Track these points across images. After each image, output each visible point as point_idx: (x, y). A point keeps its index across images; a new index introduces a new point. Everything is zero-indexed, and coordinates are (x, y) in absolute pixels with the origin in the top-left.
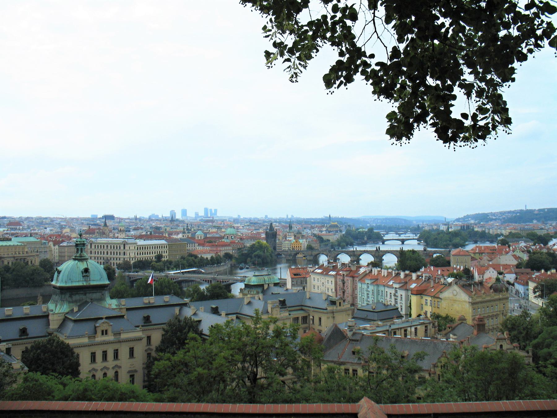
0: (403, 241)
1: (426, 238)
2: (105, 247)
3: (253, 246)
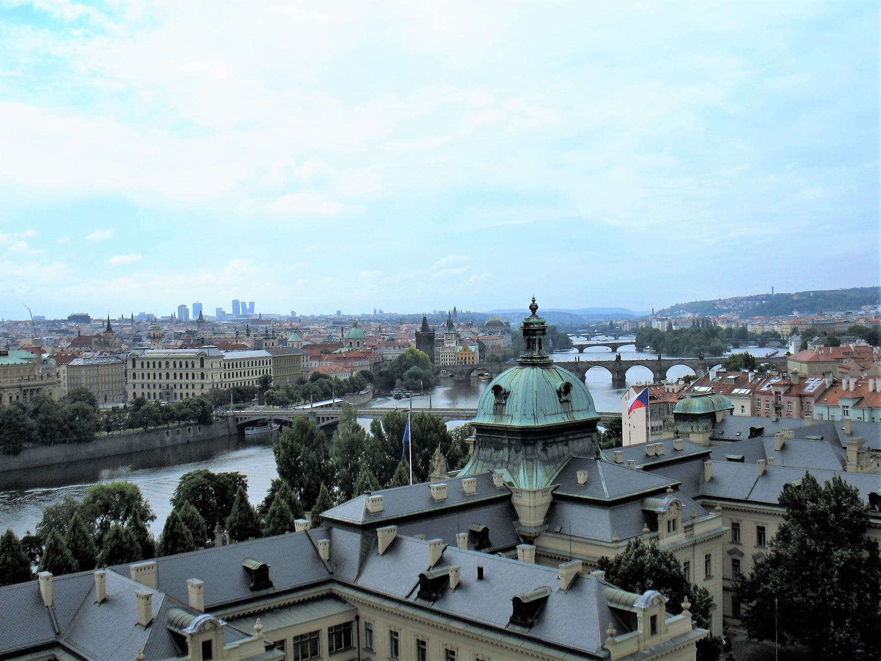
0: (614, 347)
1: (655, 342)
2: (164, 365)
3: (402, 358)
